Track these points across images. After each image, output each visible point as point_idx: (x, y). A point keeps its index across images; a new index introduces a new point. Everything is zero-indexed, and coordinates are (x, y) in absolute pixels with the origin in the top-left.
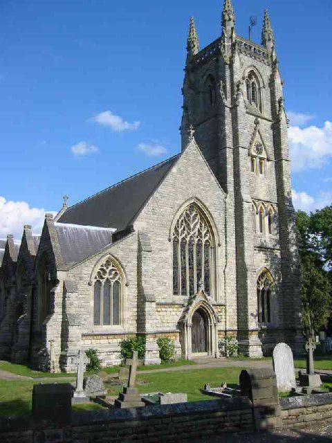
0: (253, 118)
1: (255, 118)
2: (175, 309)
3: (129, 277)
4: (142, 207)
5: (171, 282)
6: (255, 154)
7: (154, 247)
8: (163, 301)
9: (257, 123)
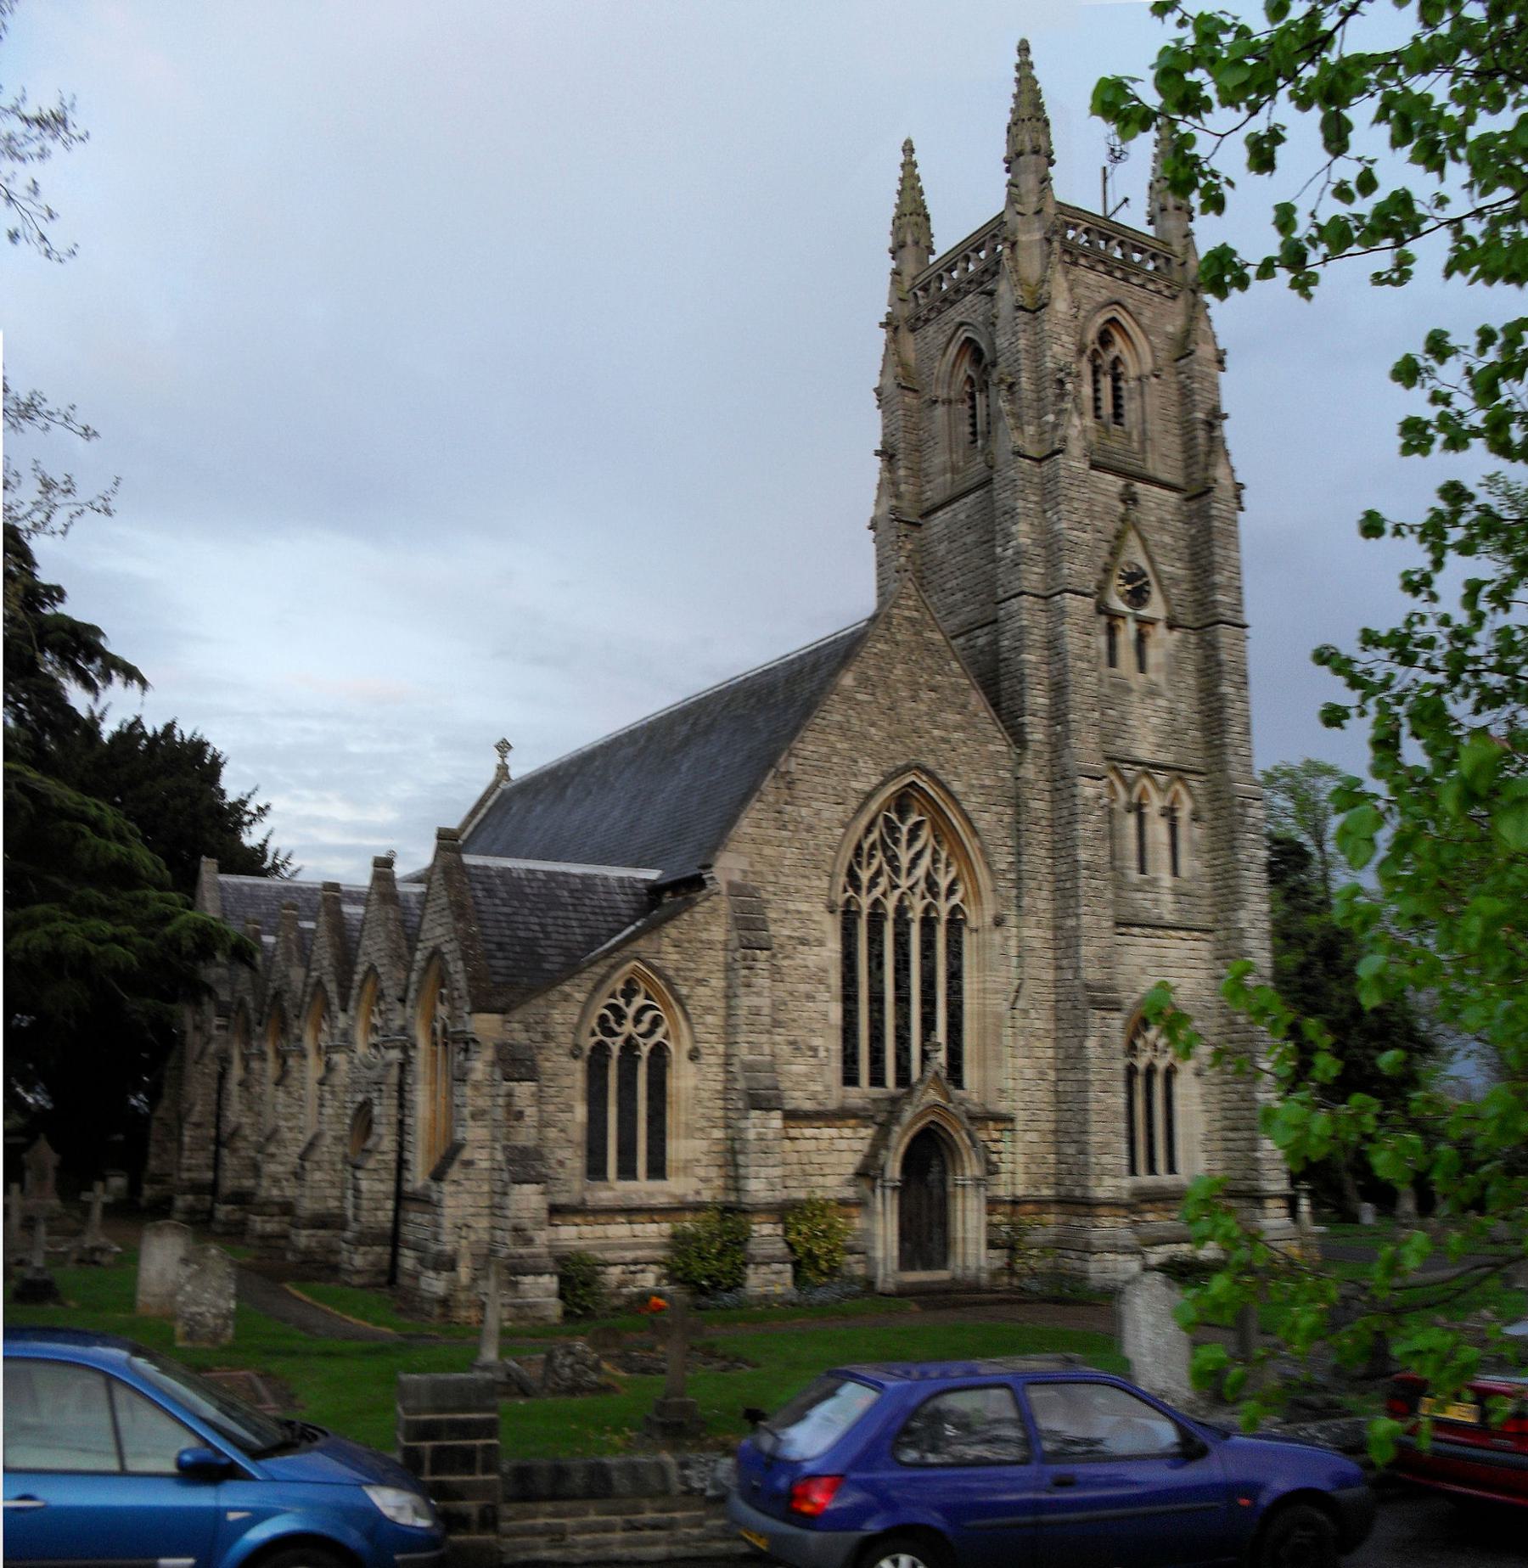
0: (1113, 483)
1: (1121, 482)
2: (847, 1132)
3: (698, 1029)
4: (901, 1250)
5: (836, 1045)
6: (1124, 608)
7: (781, 931)
8: (808, 1106)
9: (1129, 498)
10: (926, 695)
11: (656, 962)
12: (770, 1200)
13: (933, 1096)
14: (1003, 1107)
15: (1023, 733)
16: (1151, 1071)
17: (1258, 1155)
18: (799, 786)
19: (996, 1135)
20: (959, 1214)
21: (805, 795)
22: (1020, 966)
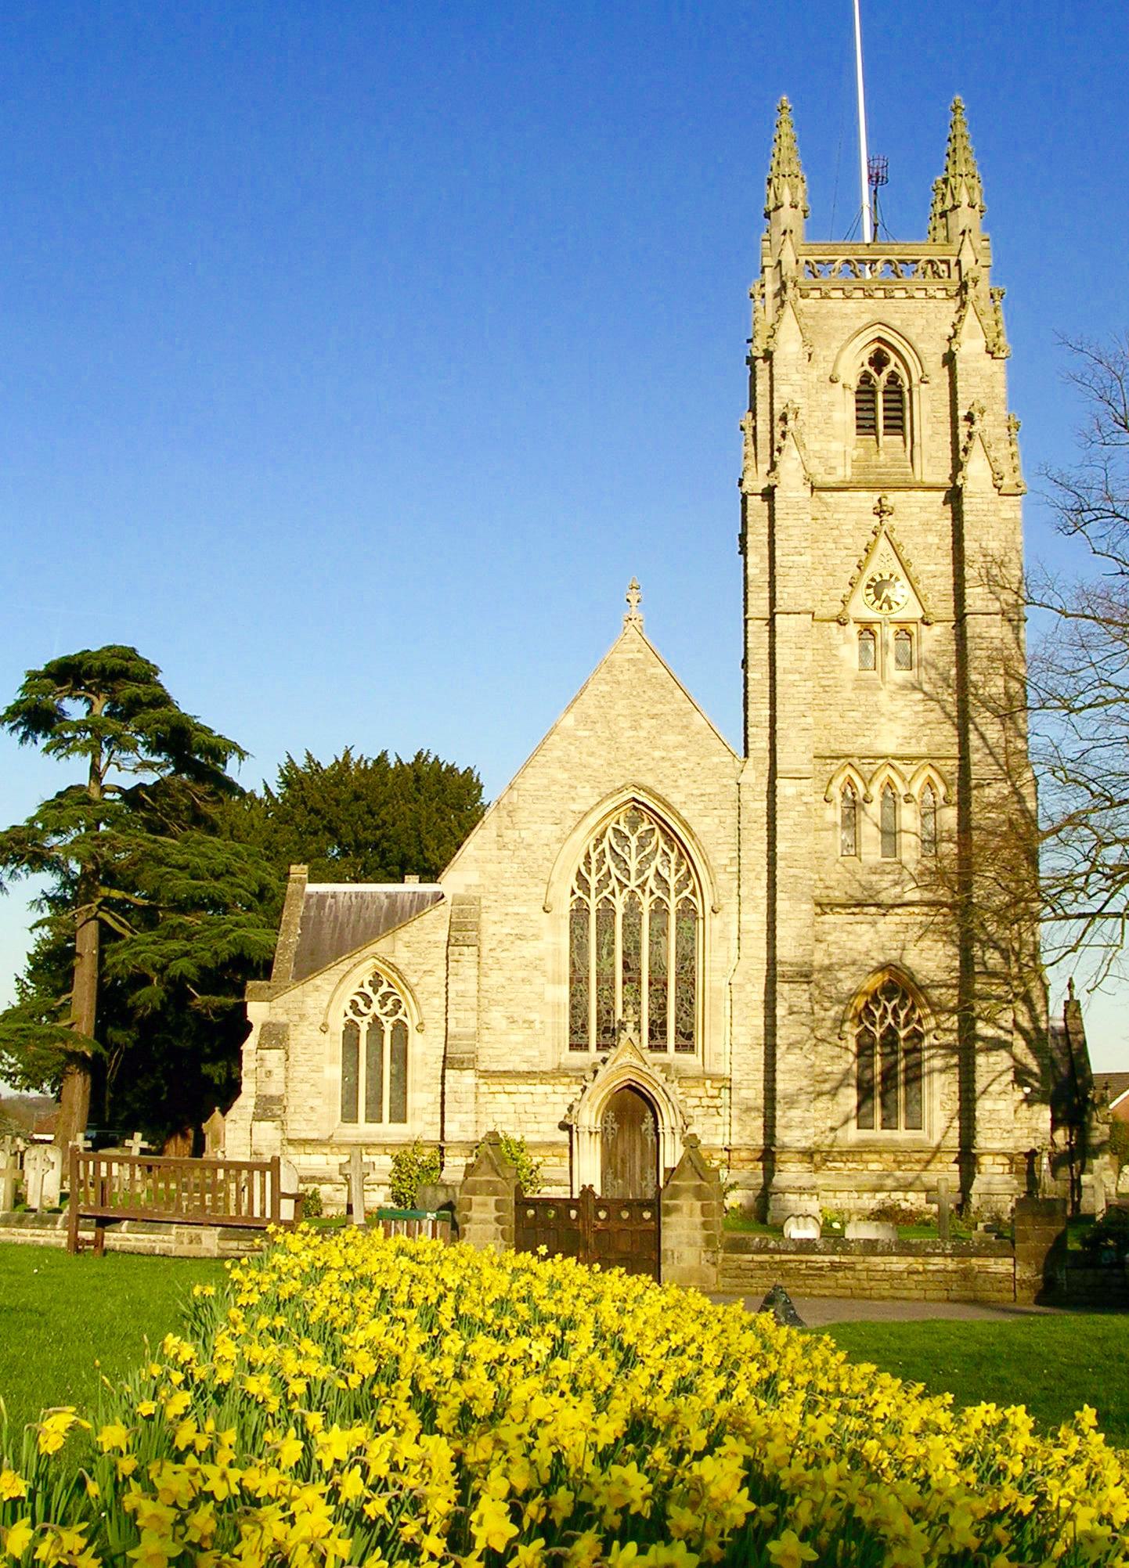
2: (560, 1089)
3: (424, 1009)
9: (880, 512)
10: (647, 723)
11: (392, 960)
21: (524, 820)
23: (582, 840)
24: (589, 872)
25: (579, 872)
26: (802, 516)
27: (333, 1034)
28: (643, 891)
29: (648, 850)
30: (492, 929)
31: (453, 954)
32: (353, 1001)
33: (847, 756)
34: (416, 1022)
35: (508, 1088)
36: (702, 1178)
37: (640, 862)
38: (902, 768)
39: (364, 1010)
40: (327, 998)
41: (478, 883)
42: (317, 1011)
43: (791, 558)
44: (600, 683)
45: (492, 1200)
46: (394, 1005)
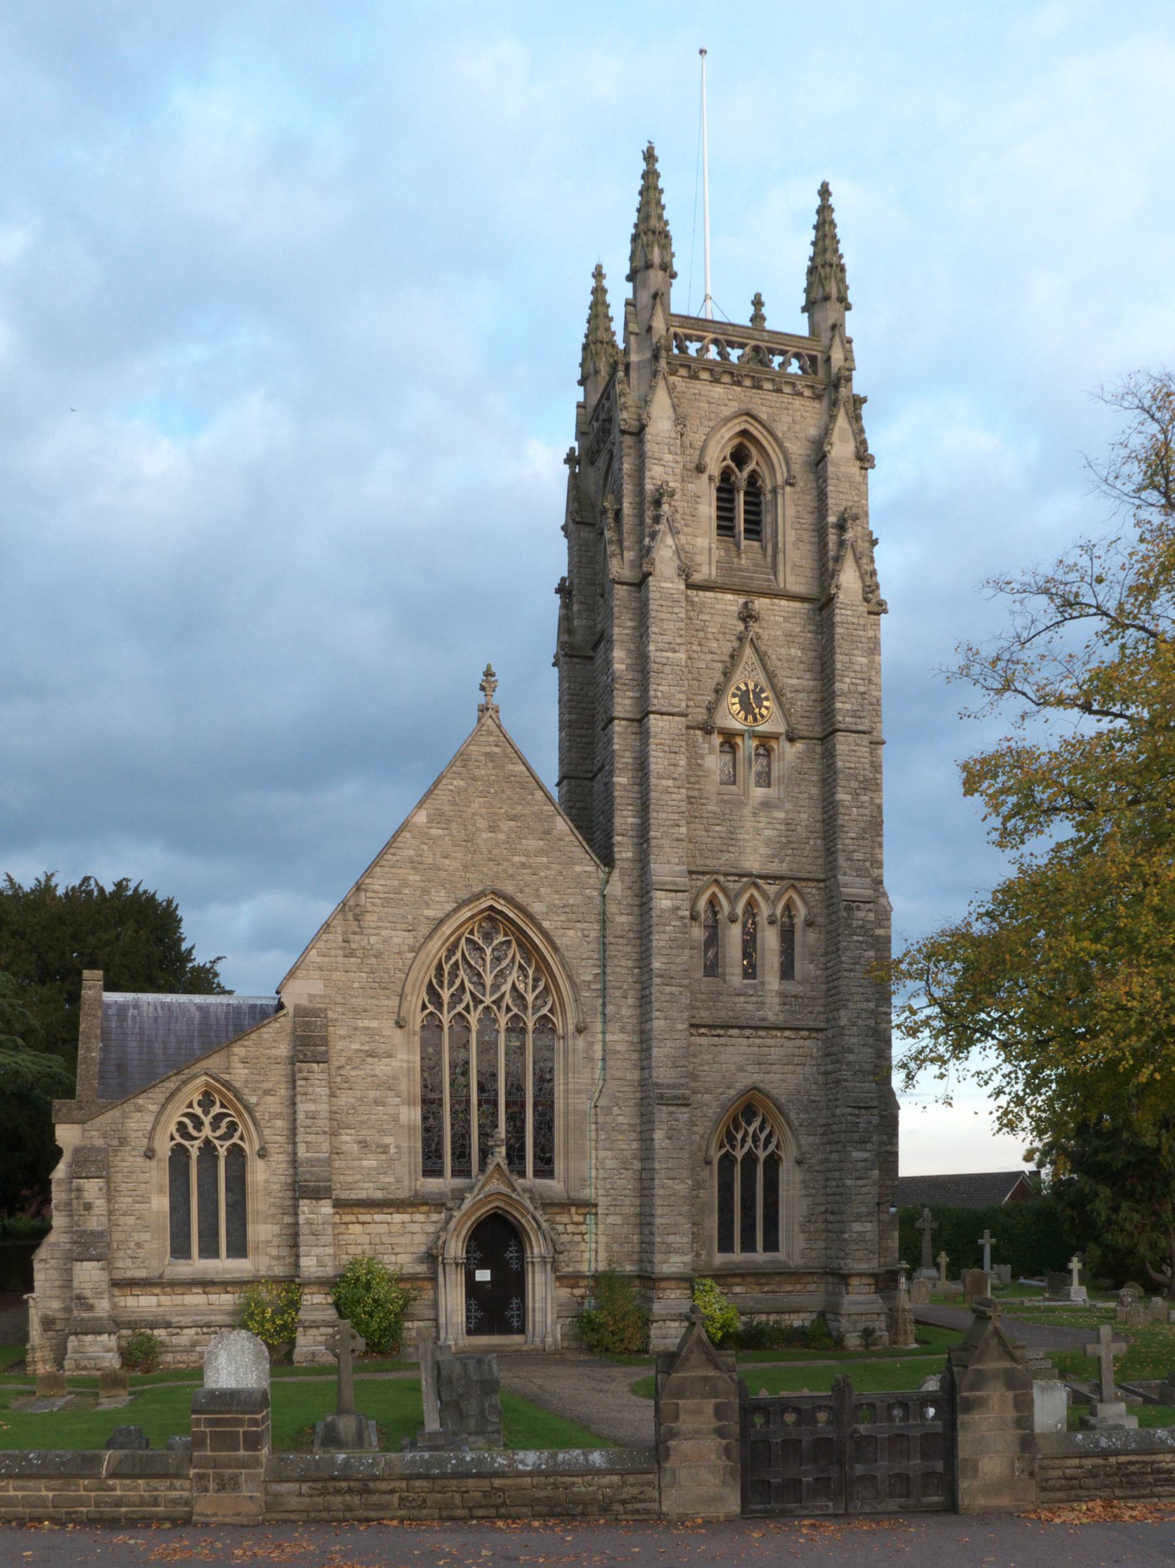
2: (419, 1217)
3: (267, 1132)
6: (737, 725)
8: (379, 1195)
9: (747, 616)
10: (505, 825)
11: (226, 1077)
12: (320, 1274)
13: (496, 1185)
14: (588, 1193)
15: (612, 852)
16: (750, 1160)
17: (846, 1236)
18: (369, 917)
19: (577, 1218)
20: (530, 1287)
21: (373, 925)
22: (604, 1069)
23: (436, 948)
24: (441, 985)
25: (430, 983)
26: (676, 610)
27: (160, 1160)
28: (499, 1008)
29: (504, 964)
30: (340, 1045)
31: (300, 1072)
32: (181, 1124)
33: (713, 873)
34: (257, 1147)
35: (362, 1218)
36: (1013, 1359)
37: (496, 976)
38: (766, 887)
39: (194, 1133)
40: (150, 1119)
41: (322, 993)
42: (140, 1134)
43: (664, 654)
44: (454, 778)
45: (709, 1405)
46: (227, 1127)
